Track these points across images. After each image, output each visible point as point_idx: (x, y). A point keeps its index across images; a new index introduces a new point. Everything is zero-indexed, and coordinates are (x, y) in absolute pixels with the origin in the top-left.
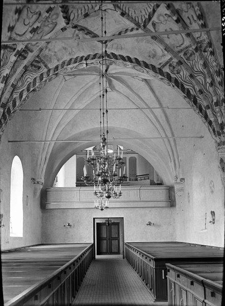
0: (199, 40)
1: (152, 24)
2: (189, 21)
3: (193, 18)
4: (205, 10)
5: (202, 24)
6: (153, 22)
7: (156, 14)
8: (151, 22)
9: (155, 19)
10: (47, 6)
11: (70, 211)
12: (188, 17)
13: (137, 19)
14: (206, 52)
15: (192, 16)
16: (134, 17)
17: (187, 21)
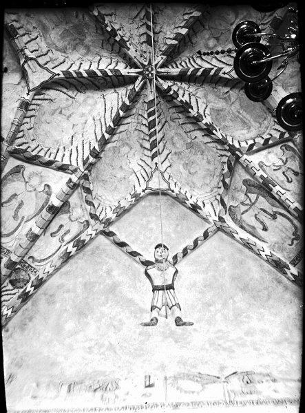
0: (30, 262)
1: (18, 166)
2: (55, 230)
3: (66, 234)
4: (280, 275)
5: (70, 252)
6: (22, 167)
7: (40, 169)
8: (19, 163)
9: (29, 169)
10: (196, 140)
11: (103, 100)
12: (61, 226)
13: (20, 134)
14: (13, 285)
15: (69, 231)
16: (21, 128)
17: (54, 227)
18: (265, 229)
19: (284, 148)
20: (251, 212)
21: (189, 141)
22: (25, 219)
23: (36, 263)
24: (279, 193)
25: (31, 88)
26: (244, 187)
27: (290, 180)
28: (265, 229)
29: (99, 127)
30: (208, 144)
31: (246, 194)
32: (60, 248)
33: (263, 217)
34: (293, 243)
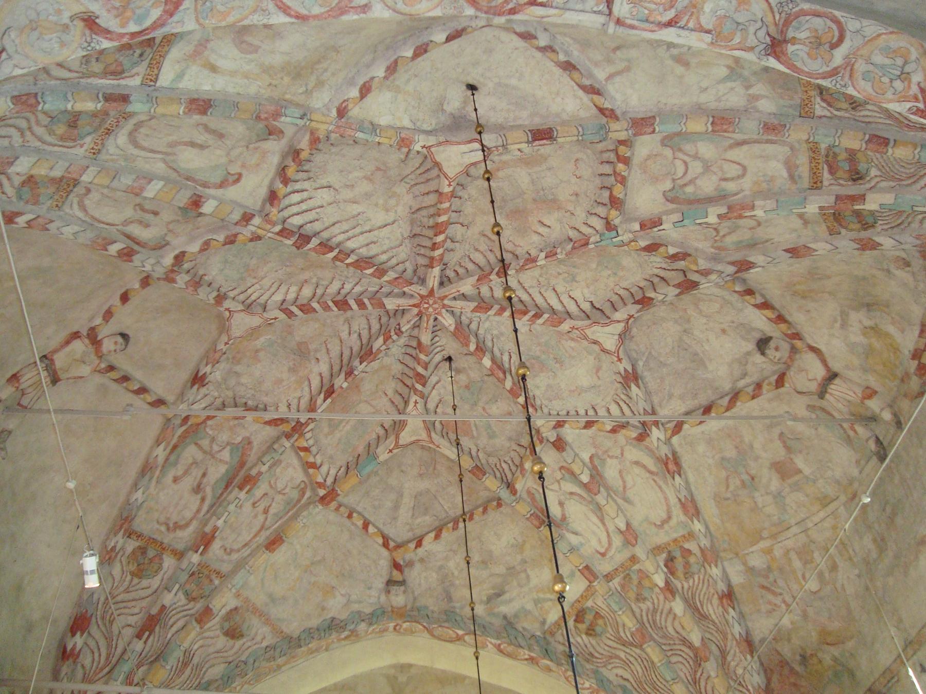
10: (313, 361)
18: (176, 480)
19: (303, 486)
20: (199, 456)
21: (312, 347)
22: (168, 158)
23: (76, 200)
24: (238, 500)
25: (433, 149)
26: (239, 439)
27: (256, 505)
28: (176, 480)
29: (345, 226)
30: (306, 383)
31: (228, 444)
32: (113, 225)
33: (197, 473)
34: (161, 524)
